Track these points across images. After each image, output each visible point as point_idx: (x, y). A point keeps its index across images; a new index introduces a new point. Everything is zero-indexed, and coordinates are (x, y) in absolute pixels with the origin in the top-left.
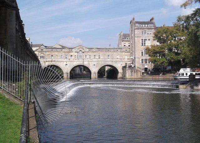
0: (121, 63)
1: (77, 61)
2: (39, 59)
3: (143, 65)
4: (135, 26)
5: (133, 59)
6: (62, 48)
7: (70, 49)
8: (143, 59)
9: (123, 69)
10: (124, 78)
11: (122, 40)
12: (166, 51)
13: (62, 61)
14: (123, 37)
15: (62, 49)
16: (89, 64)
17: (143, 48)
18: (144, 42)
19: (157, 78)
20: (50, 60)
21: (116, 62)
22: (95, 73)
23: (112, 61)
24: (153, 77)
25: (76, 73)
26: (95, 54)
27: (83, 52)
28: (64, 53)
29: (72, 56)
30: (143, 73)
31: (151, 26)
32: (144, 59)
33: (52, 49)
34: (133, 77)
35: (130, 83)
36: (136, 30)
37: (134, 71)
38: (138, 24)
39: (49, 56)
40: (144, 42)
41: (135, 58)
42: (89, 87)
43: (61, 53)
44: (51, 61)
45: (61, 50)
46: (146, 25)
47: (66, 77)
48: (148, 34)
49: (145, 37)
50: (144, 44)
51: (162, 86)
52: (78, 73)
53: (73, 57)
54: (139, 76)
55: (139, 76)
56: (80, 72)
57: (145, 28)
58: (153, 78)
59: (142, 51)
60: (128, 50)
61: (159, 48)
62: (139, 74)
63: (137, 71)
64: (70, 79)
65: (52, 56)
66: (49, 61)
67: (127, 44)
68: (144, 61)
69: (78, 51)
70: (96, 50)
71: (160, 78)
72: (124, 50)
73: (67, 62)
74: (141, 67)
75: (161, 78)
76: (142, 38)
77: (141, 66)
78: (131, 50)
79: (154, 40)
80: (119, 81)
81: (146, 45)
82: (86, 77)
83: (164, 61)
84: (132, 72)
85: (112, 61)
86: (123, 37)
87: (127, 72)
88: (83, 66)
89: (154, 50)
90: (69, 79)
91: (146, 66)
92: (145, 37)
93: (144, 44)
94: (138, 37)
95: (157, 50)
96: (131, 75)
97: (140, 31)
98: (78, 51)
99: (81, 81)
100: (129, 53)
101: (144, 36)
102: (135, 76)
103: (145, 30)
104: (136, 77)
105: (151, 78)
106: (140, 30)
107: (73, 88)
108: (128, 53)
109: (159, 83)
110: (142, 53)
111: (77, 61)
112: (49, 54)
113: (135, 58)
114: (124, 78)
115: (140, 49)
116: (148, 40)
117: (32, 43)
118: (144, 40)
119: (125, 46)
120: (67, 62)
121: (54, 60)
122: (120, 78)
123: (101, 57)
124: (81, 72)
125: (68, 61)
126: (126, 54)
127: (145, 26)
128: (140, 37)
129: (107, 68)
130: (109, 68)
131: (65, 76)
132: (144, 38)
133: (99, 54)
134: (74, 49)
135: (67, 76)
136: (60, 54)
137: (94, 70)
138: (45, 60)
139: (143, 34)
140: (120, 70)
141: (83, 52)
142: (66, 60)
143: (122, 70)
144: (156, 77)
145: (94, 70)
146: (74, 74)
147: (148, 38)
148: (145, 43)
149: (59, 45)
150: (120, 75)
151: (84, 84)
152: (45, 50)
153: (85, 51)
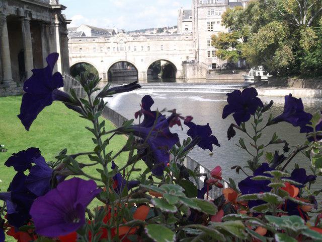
3: (210, 60)
5: (197, 50)
7: (106, 39)
9: (183, 65)
10: (185, 79)
11: (183, 20)
12: (241, 40)
14: (184, 16)
15: (94, 39)
16: (134, 59)
17: (209, 36)
18: (210, 27)
20: (78, 55)
22: (143, 72)
23: (168, 54)
25: (116, 70)
26: (142, 44)
27: (126, 42)
29: (109, 48)
30: (209, 72)
33: (80, 39)
34: (196, 77)
35: (166, 87)
40: (210, 27)
41: (198, 50)
44: (80, 57)
45: (92, 39)
48: (216, 13)
50: (210, 29)
52: (120, 70)
53: (111, 49)
54: (204, 76)
55: (204, 76)
56: (121, 68)
57: (212, 5)
60: (190, 37)
61: (229, 38)
63: (201, 68)
65: (81, 49)
66: (76, 57)
67: (190, 26)
68: (211, 54)
69: (118, 40)
72: (184, 37)
78: (193, 38)
79: (222, 25)
80: (179, 84)
81: (214, 30)
82: (131, 76)
83: (234, 56)
84: (194, 69)
85: (168, 54)
86: (184, 16)
87: (187, 69)
88: (126, 62)
89: (221, 40)
91: (214, 62)
93: (210, 29)
94: (202, 19)
95: (225, 40)
97: (206, 10)
100: (192, 41)
102: (198, 75)
105: (218, 78)
109: (214, 87)
112: (76, 47)
113: (198, 50)
114: (183, 78)
115: (205, 37)
116: (216, 23)
119: (187, 29)
122: (179, 78)
124: (123, 67)
128: (206, 19)
129: (163, 63)
130: (165, 62)
132: (210, 21)
135: (104, 77)
136: (91, 46)
137: (143, 69)
140: (179, 67)
141: (126, 42)
145: (143, 69)
147: (216, 21)
148: (212, 28)
149: (88, 26)
150: (178, 74)
153: (128, 40)
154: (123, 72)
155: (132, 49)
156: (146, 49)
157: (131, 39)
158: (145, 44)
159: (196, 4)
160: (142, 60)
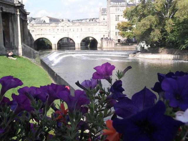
2: (31, 33)
3: (117, 37)
4: (110, 4)
5: (109, 32)
6: (50, 23)
9: (101, 40)
19: (125, 48)
23: (92, 34)
24: (123, 47)
25: (64, 42)
26: (78, 27)
27: (68, 26)
31: (123, 4)
33: (41, 24)
34: (108, 47)
36: (111, 8)
37: (109, 42)
38: (112, 3)
39: (39, 30)
40: (117, 18)
41: (110, 31)
42: (71, 57)
45: (49, 24)
46: (119, 3)
47: (54, 47)
50: (117, 20)
51: (122, 55)
52: (66, 42)
56: (67, 41)
57: (118, 5)
58: (122, 48)
60: (106, 24)
61: (127, 25)
62: (113, 44)
64: (58, 49)
65: (42, 30)
68: (117, 34)
71: (127, 48)
74: (115, 39)
75: (128, 48)
76: (116, 14)
82: (72, 46)
84: (107, 43)
85: (92, 34)
86: (103, 11)
87: (104, 43)
89: (123, 26)
90: (57, 50)
91: (119, 38)
93: (117, 20)
94: (112, 13)
96: (107, 45)
97: (115, 8)
98: (63, 26)
99: (66, 51)
101: (117, 13)
103: (118, 7)
104: (111, 47)
105: (121, 48)
106: (114, 7)
107: (116, 59)
112: (39, 29)
113: (110, 31)
115: (114, 24)
116: (120, 16)
117: (77, 84)
118: (117, 16)
119: (104, 19)
121: (43, 33)
124: (68, 41)
127: (118, 4)
128: (114, 13)
129: (91, 39)
131: (53, 47)
135: (55, 46)
136: (48, 28)
137: (78, 42)
138: (36, 34)
139: (116, 10)
140: (99, 41)
141: (68, 26)
143: (101, 41)
144: (124, 47)
145: (78, 42)
146: (61, 43)
151: (67, 54)
152: (35, 25)
155: (72, 30)
156: (80, 30)
157: (71, 24)
158: (79, 28)
159: (109, 5)
160: (78, 37)
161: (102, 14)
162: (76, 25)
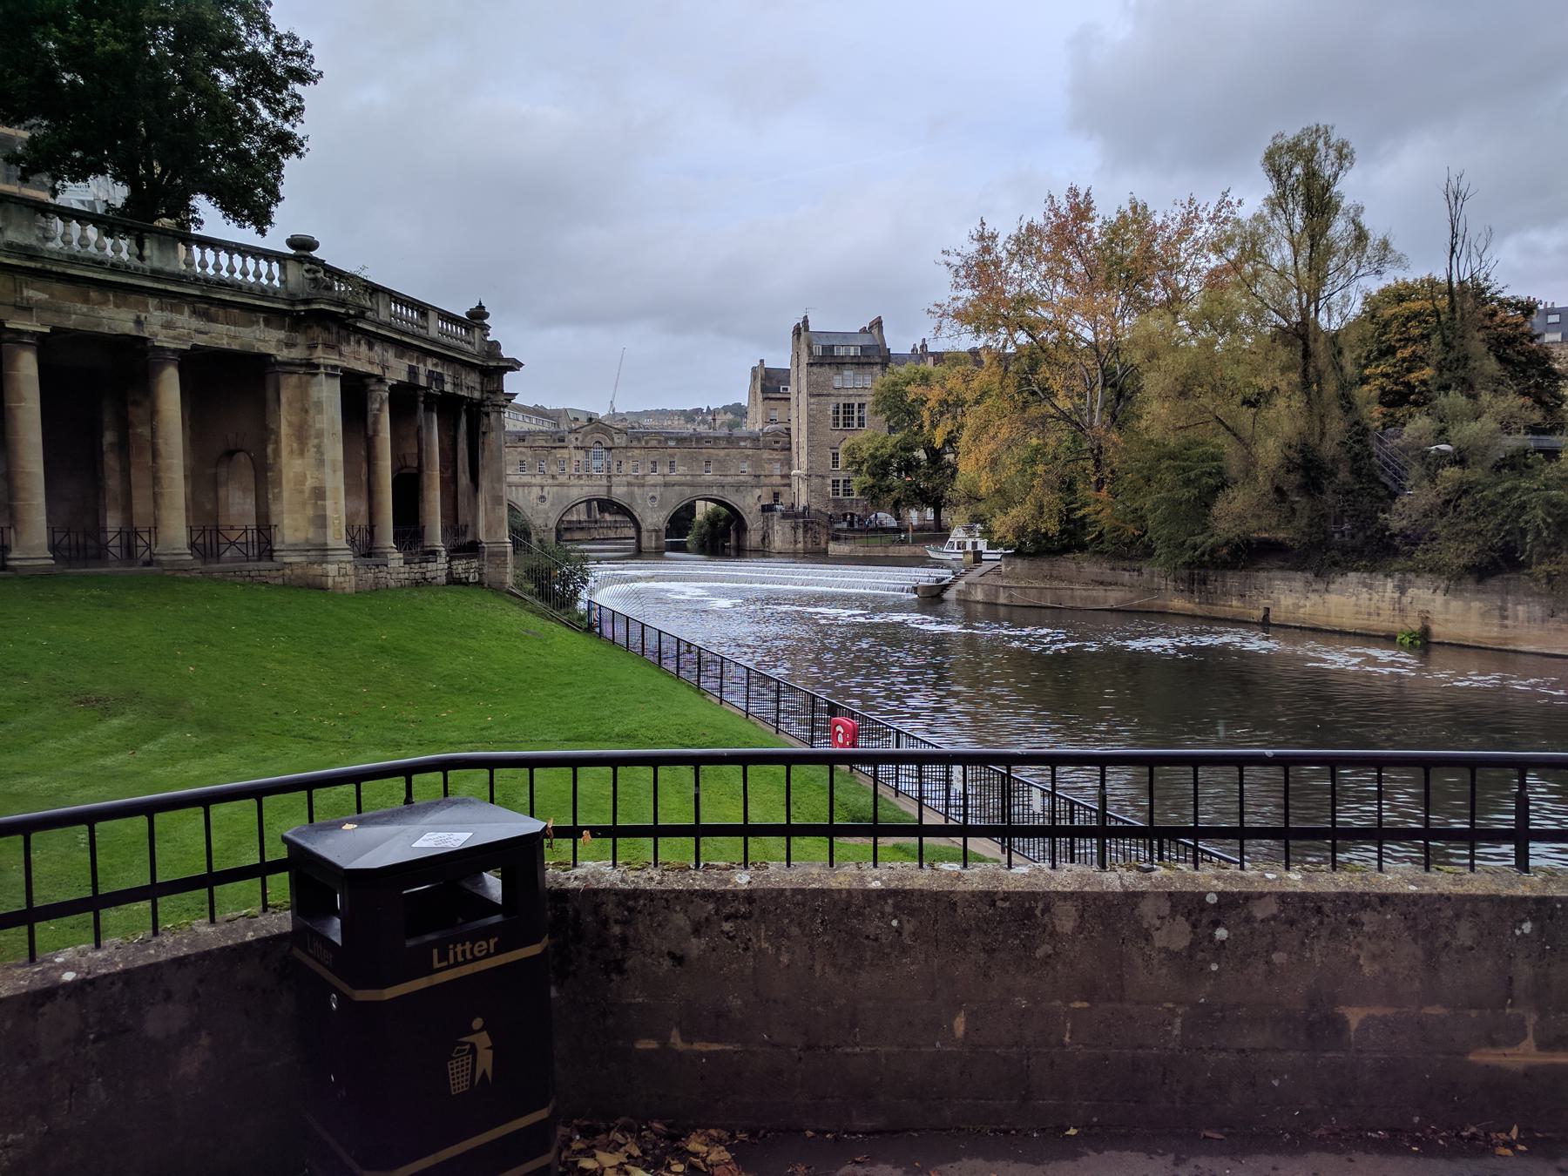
0: (758, 492)
1: (582, 482)
8: (838, 481)
13: (523, 485)
16: (632, 495)
21: (738, 487)
26: (654, 455)
28: (529, 452)
32: (841, 479)
36: (815, 369)
43: (521, 453)
49: (844, 395)
52: (580, 522)
57: (847, 360)
59: (834, 451)
68: (841, 488)
69: (589, 442)
70: (660, 442)
73: (542, 487)
77: (830, 508)
84: (795, 528)
87: (776, 527)
92: (844, 395)
94: (819, 395)
108: (786, 452)
110: (835, 456)
111: (582, 482)
120: (542, 487)
123: (681, 469)
125: (550, 481)
126: (776, 455)
128: (828, 395)
132: (842, 401)
133: (671, 456)
134: (572, 437)
141: (609, 449)
142: (538, 480)
154: (589, 528)
160: (653, 498)
161: (765, 396)
162: (647, 442)
